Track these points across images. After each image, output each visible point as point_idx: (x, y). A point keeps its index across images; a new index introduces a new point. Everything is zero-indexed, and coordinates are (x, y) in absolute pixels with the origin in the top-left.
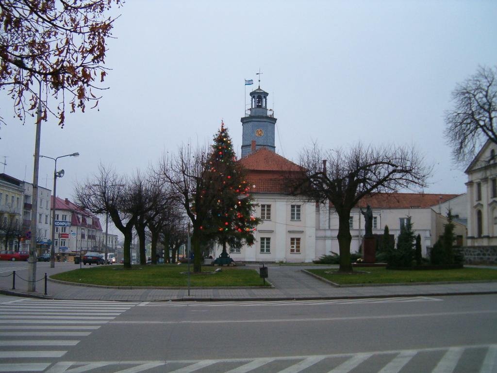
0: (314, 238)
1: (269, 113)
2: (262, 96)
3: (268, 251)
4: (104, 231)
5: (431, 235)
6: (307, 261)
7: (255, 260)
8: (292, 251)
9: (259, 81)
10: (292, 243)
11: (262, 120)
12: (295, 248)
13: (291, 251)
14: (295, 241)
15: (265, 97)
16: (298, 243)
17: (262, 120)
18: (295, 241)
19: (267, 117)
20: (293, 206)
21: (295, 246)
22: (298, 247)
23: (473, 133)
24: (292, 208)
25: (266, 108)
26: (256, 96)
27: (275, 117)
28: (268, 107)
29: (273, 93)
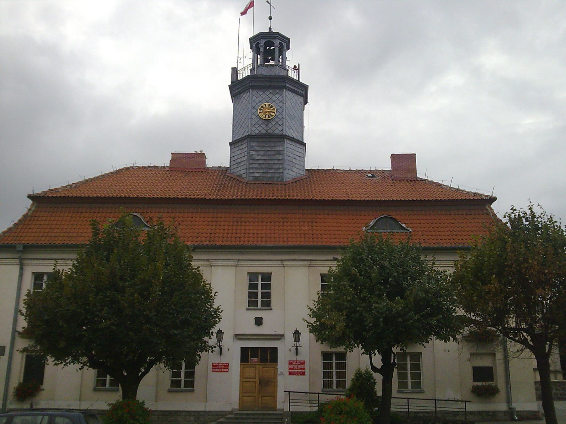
9: (270, 18)
26: (262, 42)
28: (290, 64)
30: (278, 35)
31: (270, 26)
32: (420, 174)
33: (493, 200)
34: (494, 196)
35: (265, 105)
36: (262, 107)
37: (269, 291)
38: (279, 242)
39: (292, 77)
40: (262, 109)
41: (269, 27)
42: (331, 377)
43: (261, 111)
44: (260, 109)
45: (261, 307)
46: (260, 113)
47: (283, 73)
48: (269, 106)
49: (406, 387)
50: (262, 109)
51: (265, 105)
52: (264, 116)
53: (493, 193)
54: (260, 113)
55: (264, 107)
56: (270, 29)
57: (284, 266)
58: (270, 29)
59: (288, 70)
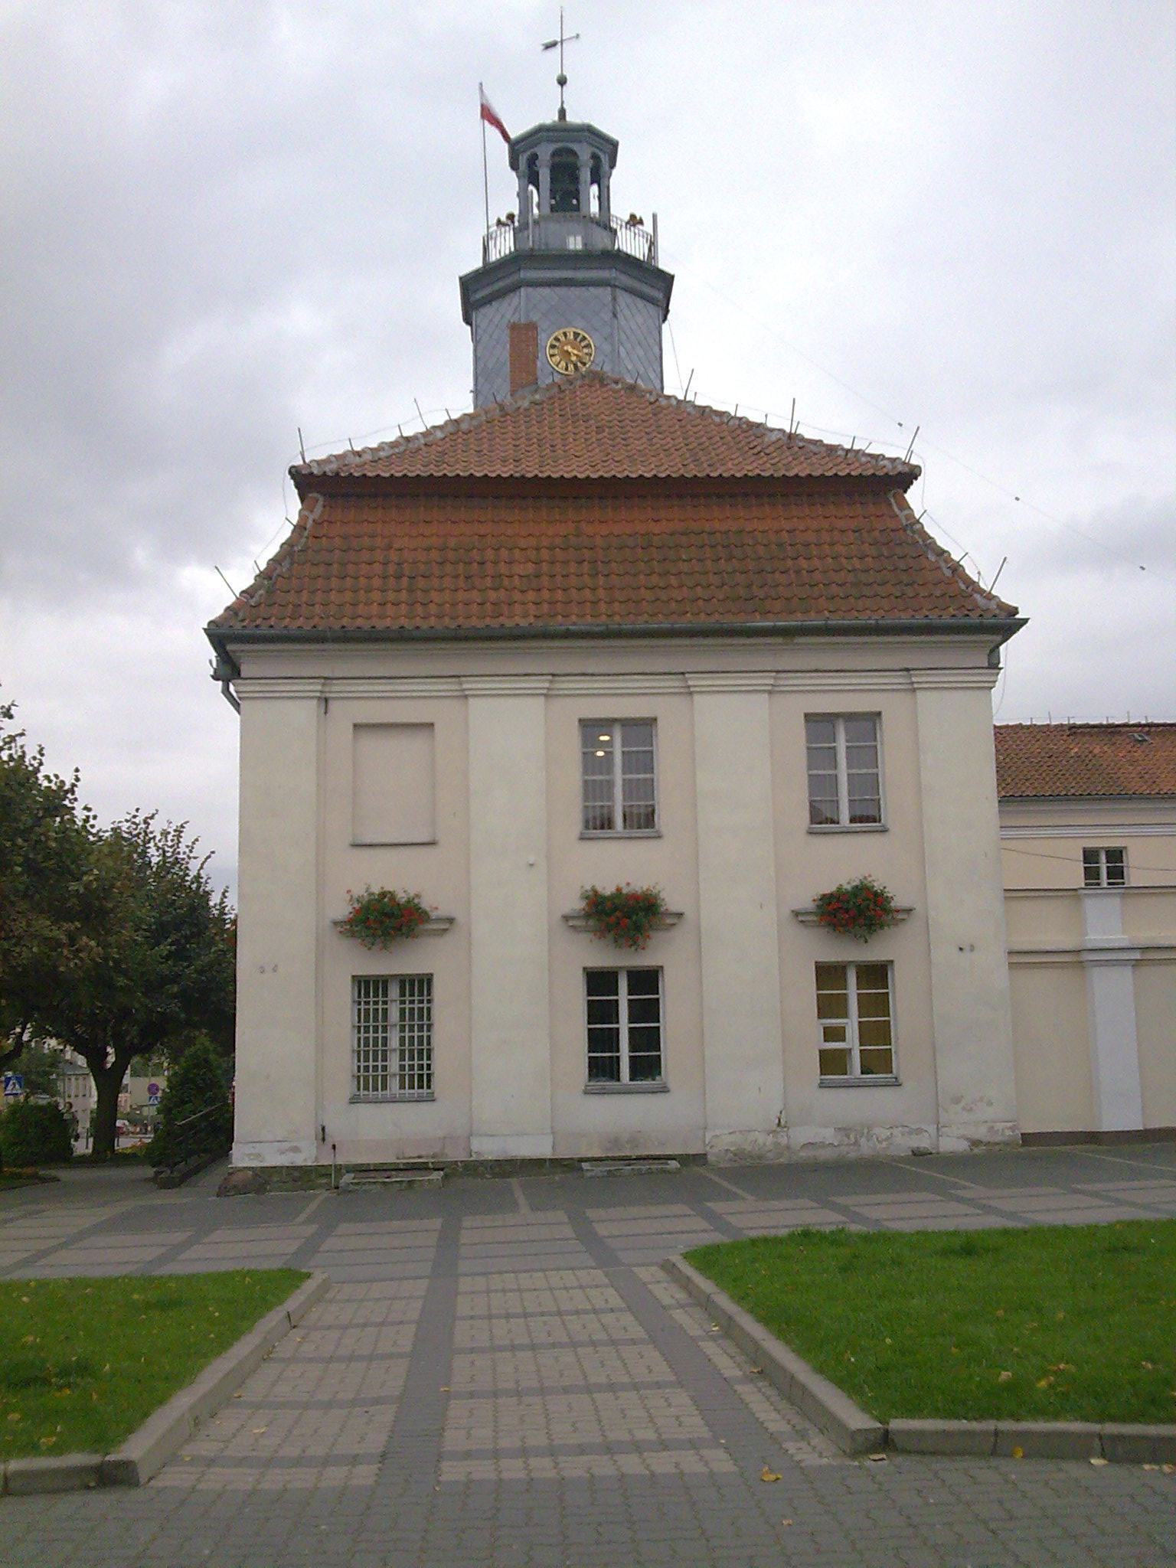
0: (992, 962)
1: (631, 244)
2: (584, 153)
3: (647, 1067)
4: (365, 1475)
5: (763, 1480)
6: (952, 1143)
7: (541, 1148)
8: (832, 1063)
9: (562, 81)
10: (831, 1006)
11: (581, 275)
12: (852, 1041)
13: (825, 1068)
14: (852, 991)
15: (599, 176)
16: (877, 1005)
17: (581, 275)
18: (852, 991)
19: (611, 228)
20: (819, 723)
21: (851, 1024)
22: (877, 1033)
23: (984, 1202)
24: (811, 737)
25: (604, 223)
26: (545, 152)
27: (664, 264)
28: (620, 211)
29: (561, 1376)
30: (589, 133)
31: (562, 103)
32: (673, 386)
33: (908, 475)
34: (914, 461)
35: (565, 334)
36: (557, 339)
37: (860, 1020)
38: (440, 617)
39: (633, 254)
40: (557, 344)
41: (559, 106)
42: (612, 1071)
43: (556, 351)
44: (553, 347)
45: (862, 1073)
46: (552, 356)
47: (601, 241)
48: (575, 339)
49: (615, 1075)
50: (557, 344)
51: (565, 334)
52: (563, 364)
53: (910, 452)
54: (552, 356)
55: (562, 339)
56: (562, 113)
57: (466, 697)
58: (562, 113)
59: (614, 232)
